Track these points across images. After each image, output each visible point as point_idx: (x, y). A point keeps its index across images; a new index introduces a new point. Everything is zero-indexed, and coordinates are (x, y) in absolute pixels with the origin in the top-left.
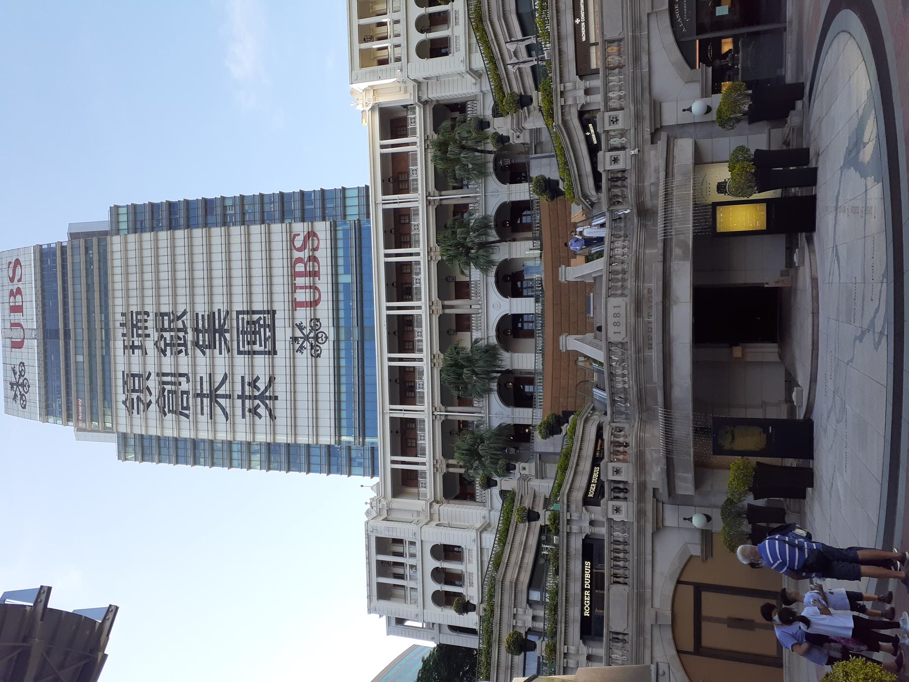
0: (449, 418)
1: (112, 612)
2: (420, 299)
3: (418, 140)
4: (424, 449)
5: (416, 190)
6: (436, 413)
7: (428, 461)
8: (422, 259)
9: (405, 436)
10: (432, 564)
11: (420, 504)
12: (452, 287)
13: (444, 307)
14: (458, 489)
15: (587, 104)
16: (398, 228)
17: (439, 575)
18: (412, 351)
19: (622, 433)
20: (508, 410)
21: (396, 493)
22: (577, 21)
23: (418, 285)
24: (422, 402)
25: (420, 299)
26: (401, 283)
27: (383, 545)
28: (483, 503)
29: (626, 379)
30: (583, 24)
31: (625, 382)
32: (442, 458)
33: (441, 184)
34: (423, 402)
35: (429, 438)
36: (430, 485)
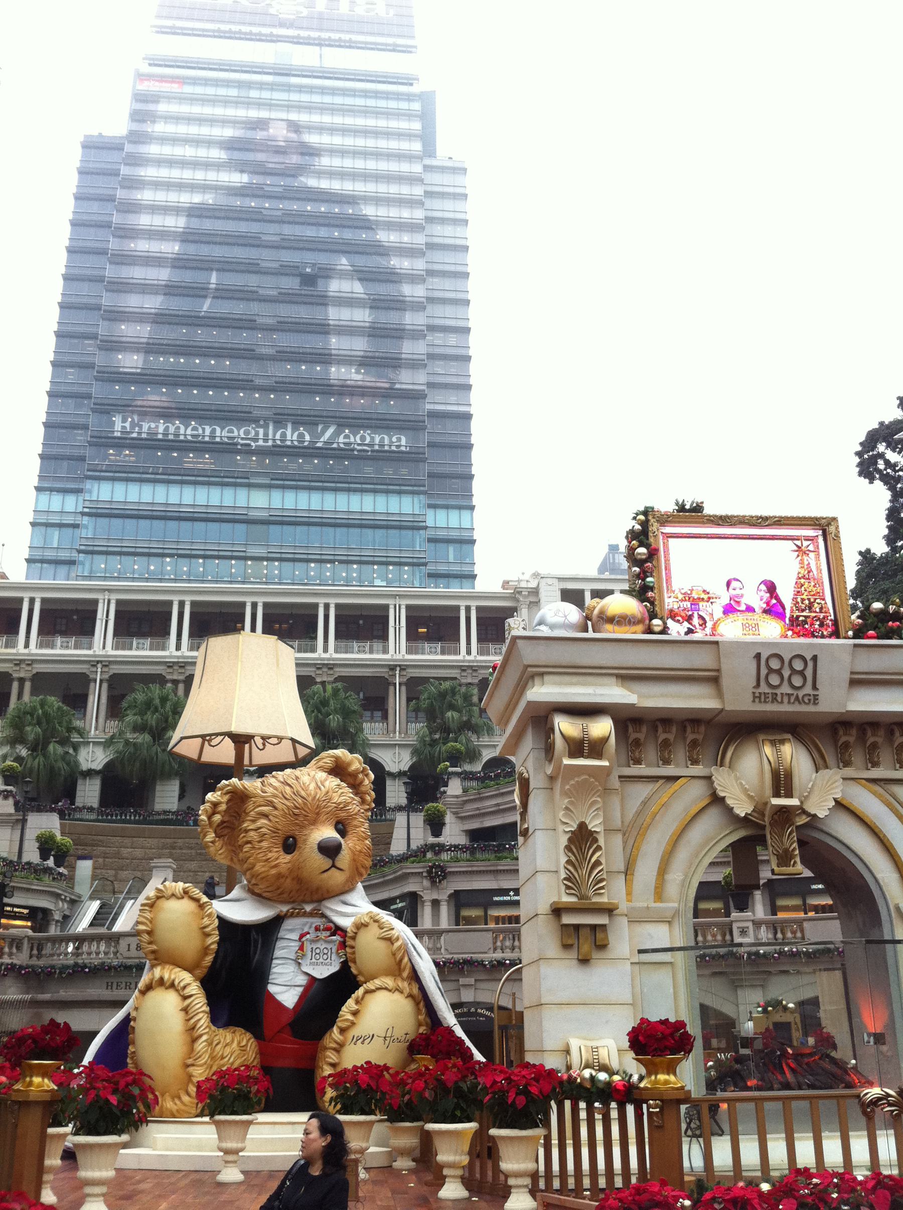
0: (92, 684)
2: (336, 651)
3: (471, 658)
5: (409, 651)
6: (99, 666)
8: (462, 656)
9: (68, 618)
13: (22, 681)
15: (423, 902)
19: (14, 950)
22: (512, 893)
23: (356, 649)
24: (41, 645)
25: (336, 651)
29: (94, 956)
30: (509, 898)
31: (89, 954)
32: (34, 671)
33: (414, 686)
34: (117, 648)
35: (64, 651)
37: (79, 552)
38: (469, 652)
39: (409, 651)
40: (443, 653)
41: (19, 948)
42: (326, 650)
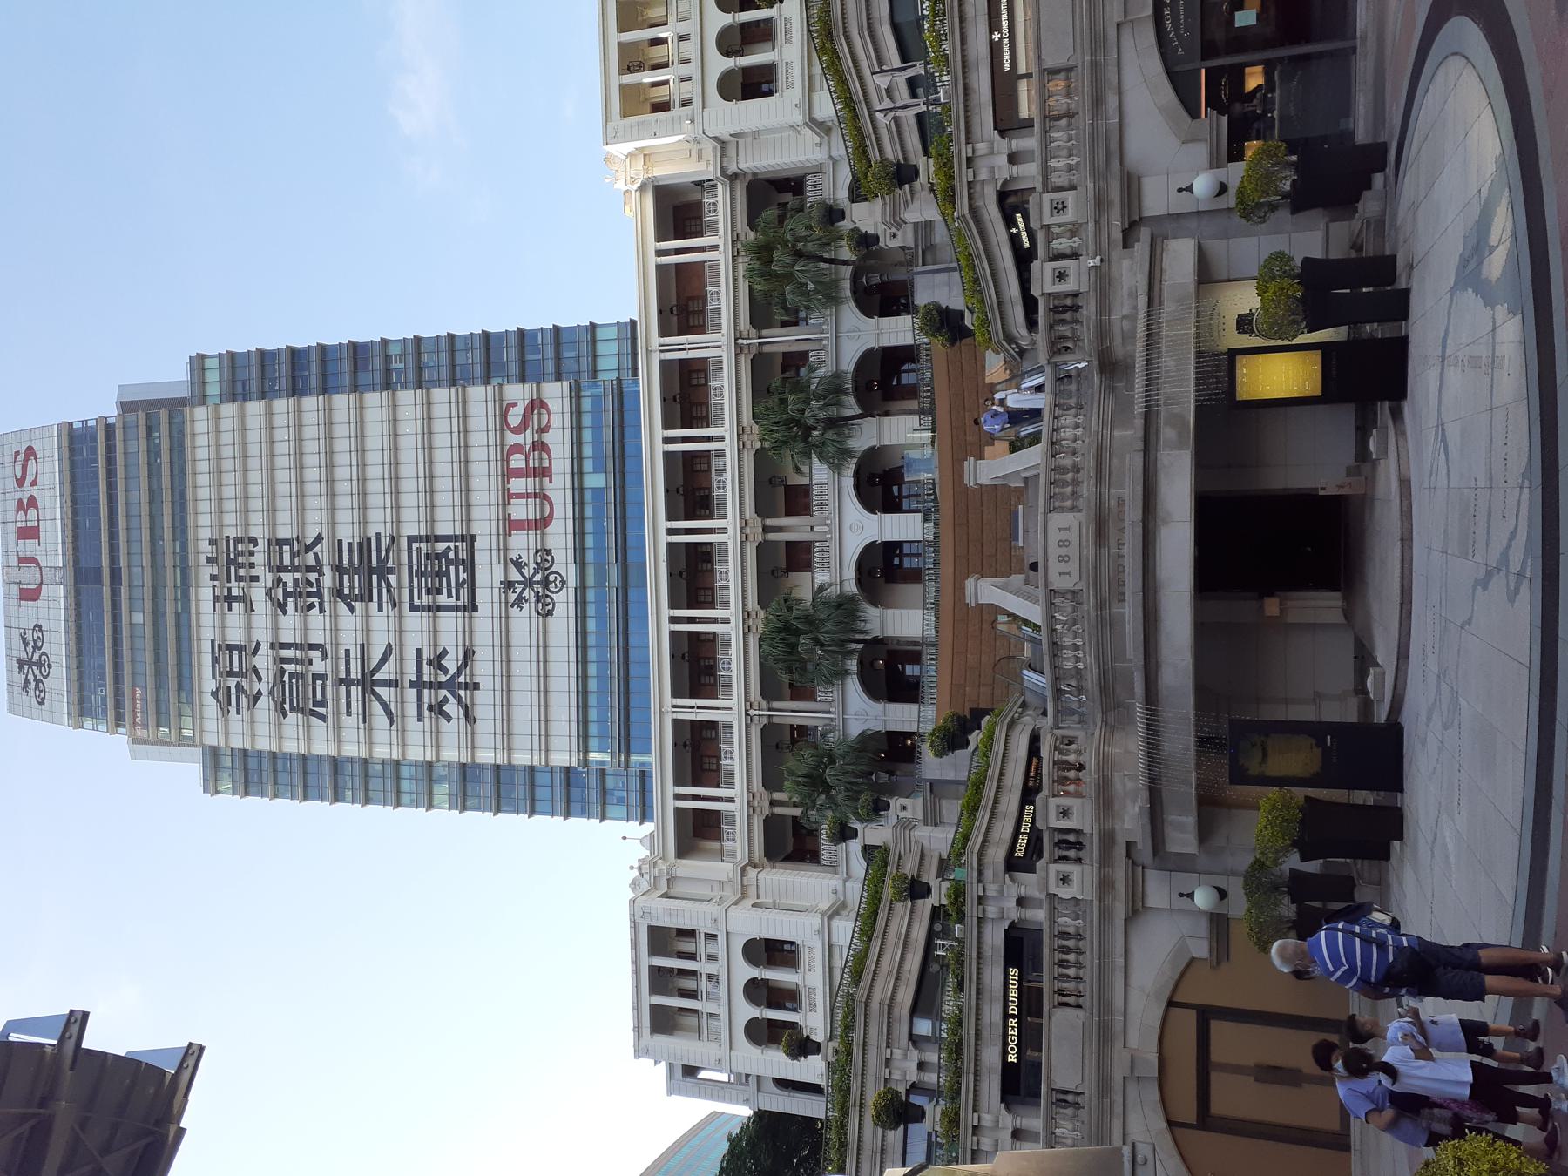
0: (775, 720)
1: (192, 1055)
2: (724, 516)
3: (721, 242)
4: (731, 774)
5: (717, 328)
6: (751, 712)
7: (738, 795)
8: (729, 446)
9: (698, 751)
10: (746, 972)
11: (724, 870)
12: (781, 495)
13: (766, 529)
14: (791, 844)
15: (1013, 179)
16: (687, 394)
17: (757, 991)
18: (711, 605)
19: (1074, 746)
20: (876, 708)
21: (683, 851)
22: (996, 36)
23: (721, 492)
24: (728, 694)
25: (724, 516)
26: (691, 488)
27: (661, 939)
28: (833, 868)
29: (1080, 653)
30: (1006, 41)
31: (1077, 659)
32: (762, 789)
33: (760, 316)
34: (730, 694)
35: (739, 756)
36: (742, 836)
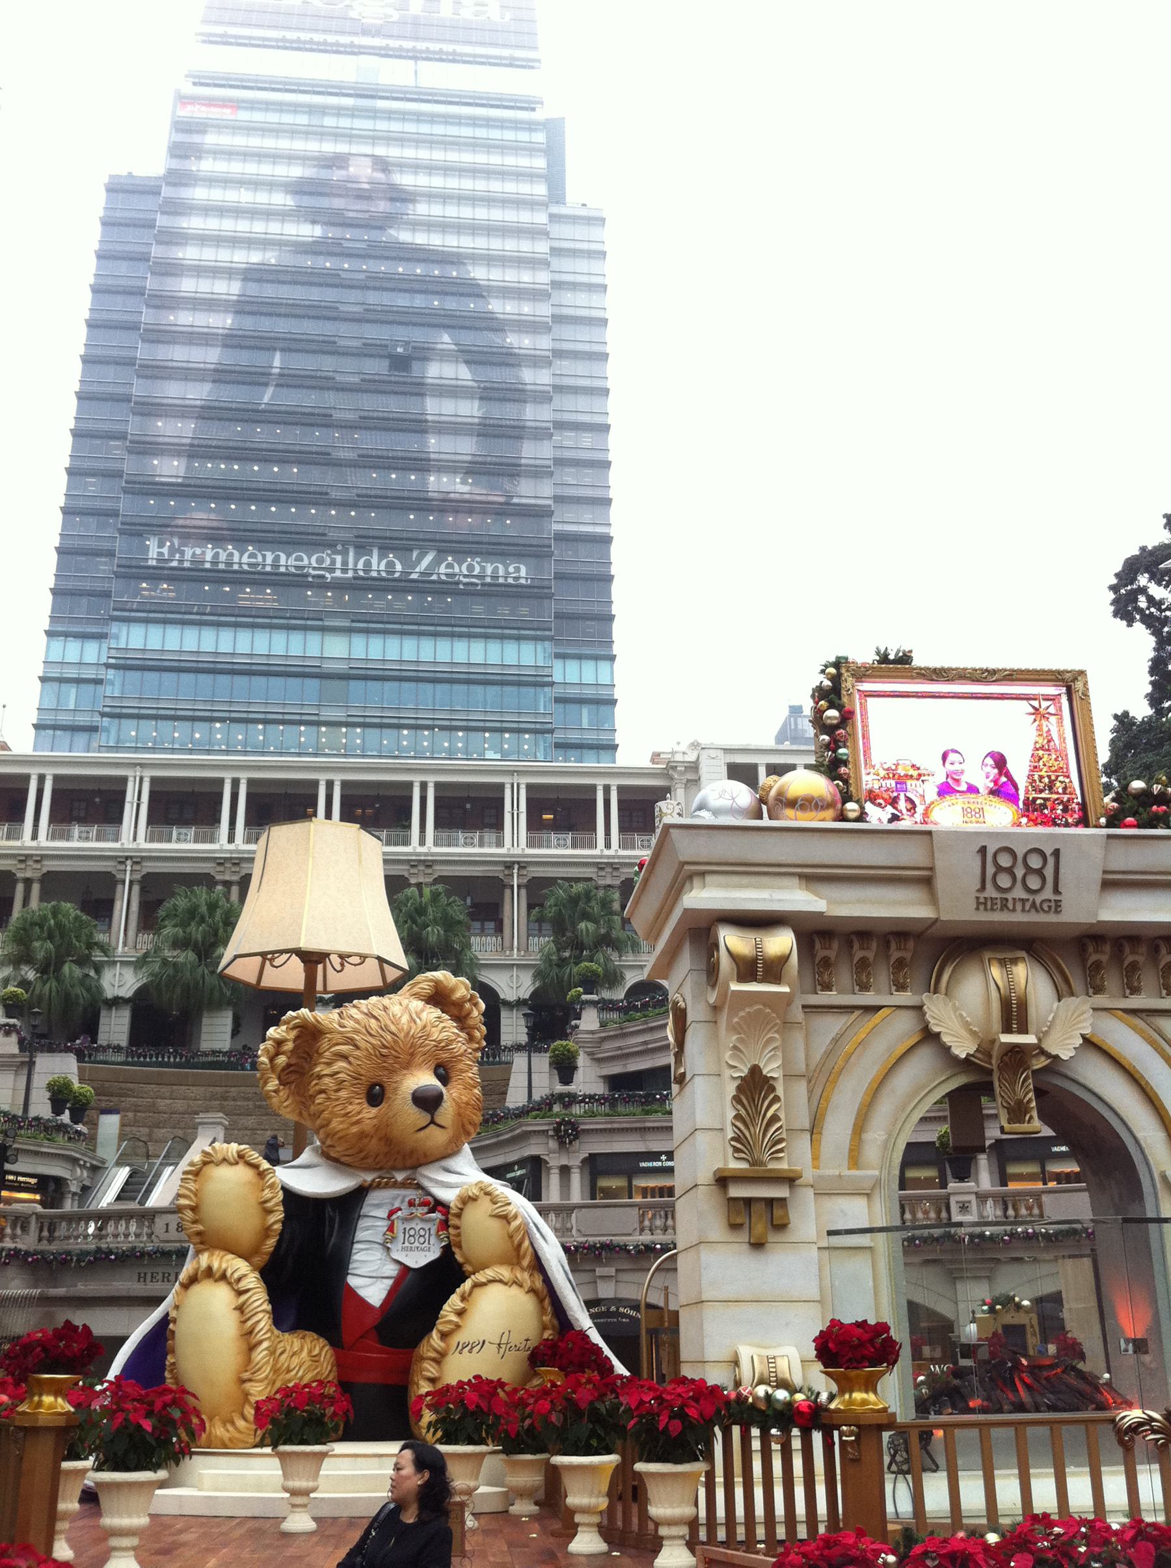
0: (119, 887)
2: (436, 844)
3: (611, 852)
5: (531, 844)
6: (129, 862)
8: (599, 850)
9: (88, 801)
13: (28, 882)
15: (549, 1169)
19: (19, 1231)
22: (663, 1157)
23: (462, 841)
24: (53, 836)
25: (436, 844)
29: (122, 1238)
30: (660, 1164)
31: (116, 1236)
32: (45, 870)
33: (537, 889)
34: (152, 840)
35: (83, 844)
37: (103, 715)
38: (608, 845)
39: (531, 844)
40: (574, 846)
41: (24, 1229)
42: (422, 842)
